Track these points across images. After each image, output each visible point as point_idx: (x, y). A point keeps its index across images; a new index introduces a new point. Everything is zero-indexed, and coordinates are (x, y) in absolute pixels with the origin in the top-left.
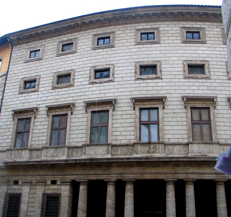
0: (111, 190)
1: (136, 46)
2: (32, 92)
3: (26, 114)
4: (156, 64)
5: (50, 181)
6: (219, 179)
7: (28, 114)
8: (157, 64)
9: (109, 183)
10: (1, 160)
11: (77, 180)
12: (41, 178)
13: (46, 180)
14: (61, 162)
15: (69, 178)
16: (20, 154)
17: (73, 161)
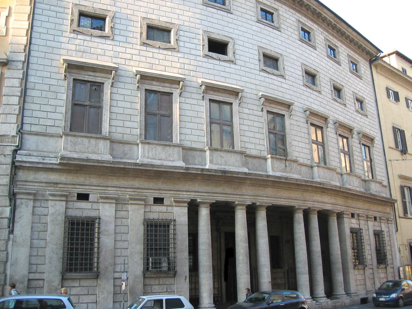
0: (299, 217)
1: (257, 23)
2: (100, 36)
3: (91, 73)
4: (279, 57)
5: (153, 198)
6: (263, 203)
7: (97, 74)
8: (280, 58)
9: (201, 205)
11: (259, 203)
12: (136, 193)
13: (69, 192)
14: (177, 169)
15: (187, 196)
16: (94, 146)
17: (197, 171)
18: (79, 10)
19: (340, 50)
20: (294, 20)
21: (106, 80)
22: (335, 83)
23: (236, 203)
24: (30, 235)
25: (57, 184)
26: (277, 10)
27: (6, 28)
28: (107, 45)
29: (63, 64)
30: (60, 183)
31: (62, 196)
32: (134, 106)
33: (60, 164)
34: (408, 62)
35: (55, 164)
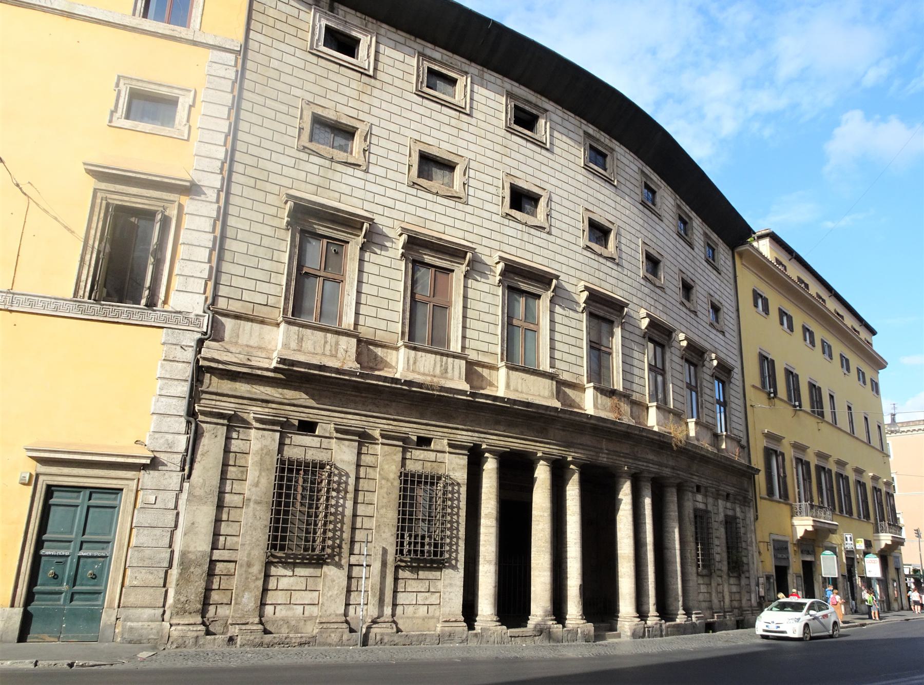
0: (542, 473)
10: (1, 292)
11: (487, 445)
12: (390, 427)
15: (466, 437)
18: (313, 113)
19: (694, 224)
20: (636, 169)
21: (353, 237)
22: (685, 276)
23: (538, 455)
24: (218, 485)
25: (267, 402)
26: (612, 150)
27: (187, 126)
28: (352, 178)
29: (286, 203)
30: (273, 402)
31: (273, 423)
32: (393, 284)
33: (275, 370)
34: (786, 251)
35: (267, 370)
